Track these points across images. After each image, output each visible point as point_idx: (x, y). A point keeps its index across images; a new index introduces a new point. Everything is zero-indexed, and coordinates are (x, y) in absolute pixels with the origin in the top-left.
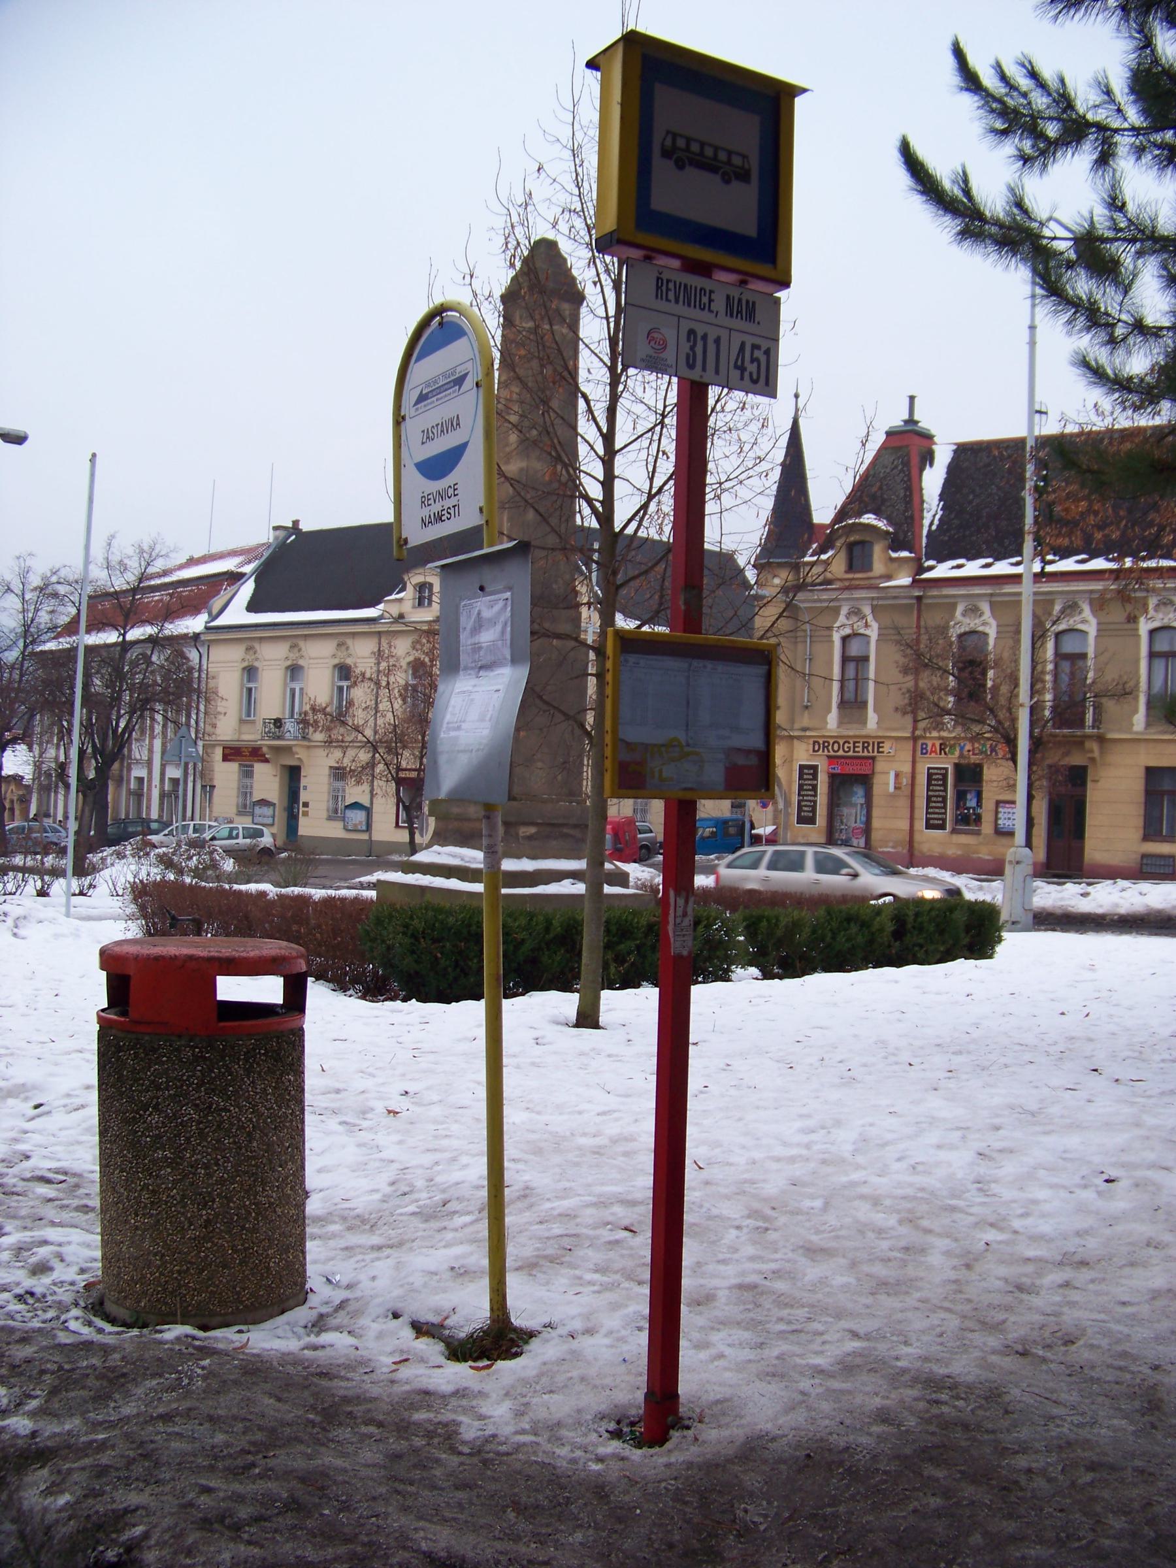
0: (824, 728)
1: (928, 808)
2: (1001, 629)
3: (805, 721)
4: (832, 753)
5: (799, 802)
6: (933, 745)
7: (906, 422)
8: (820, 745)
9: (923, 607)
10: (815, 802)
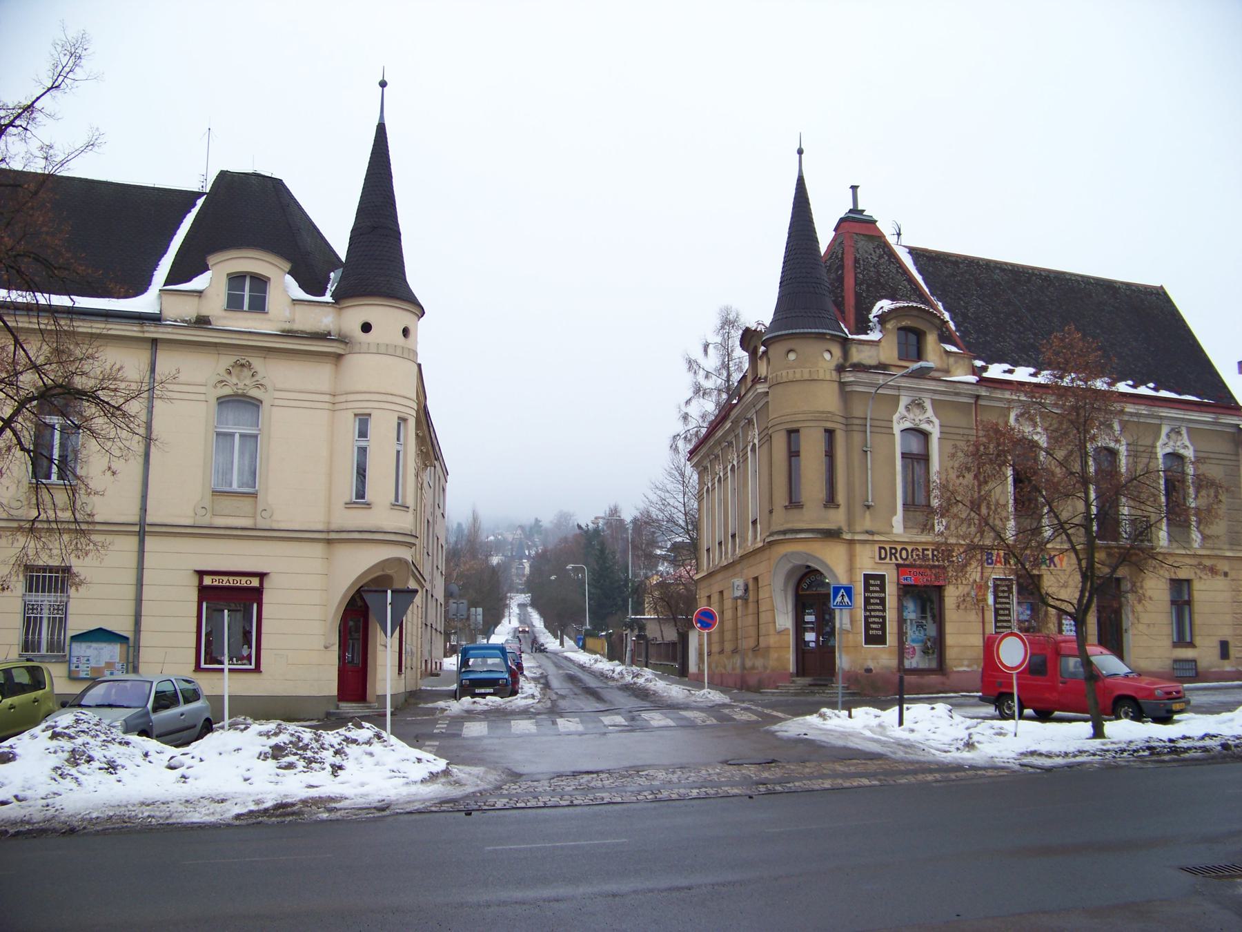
0: (890, 533)
1: (996, 621)
2: (945, 430)
3: (867, 522)
4: (900, 561)
5: (866, 618)
6: (998, 554)
7: (850, 211)
8: (888, 551)
9: (978, 407)
10: (884, 618)
